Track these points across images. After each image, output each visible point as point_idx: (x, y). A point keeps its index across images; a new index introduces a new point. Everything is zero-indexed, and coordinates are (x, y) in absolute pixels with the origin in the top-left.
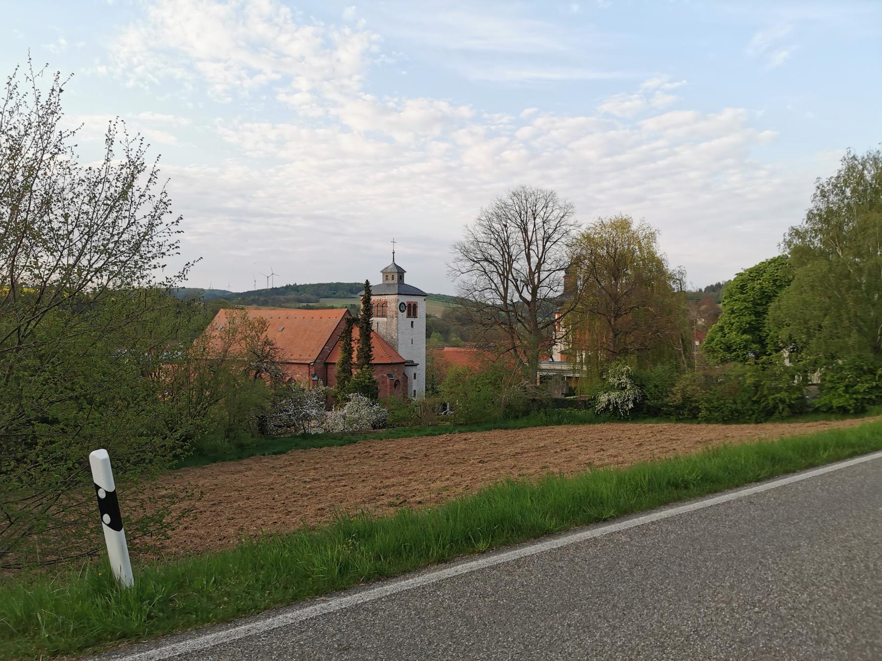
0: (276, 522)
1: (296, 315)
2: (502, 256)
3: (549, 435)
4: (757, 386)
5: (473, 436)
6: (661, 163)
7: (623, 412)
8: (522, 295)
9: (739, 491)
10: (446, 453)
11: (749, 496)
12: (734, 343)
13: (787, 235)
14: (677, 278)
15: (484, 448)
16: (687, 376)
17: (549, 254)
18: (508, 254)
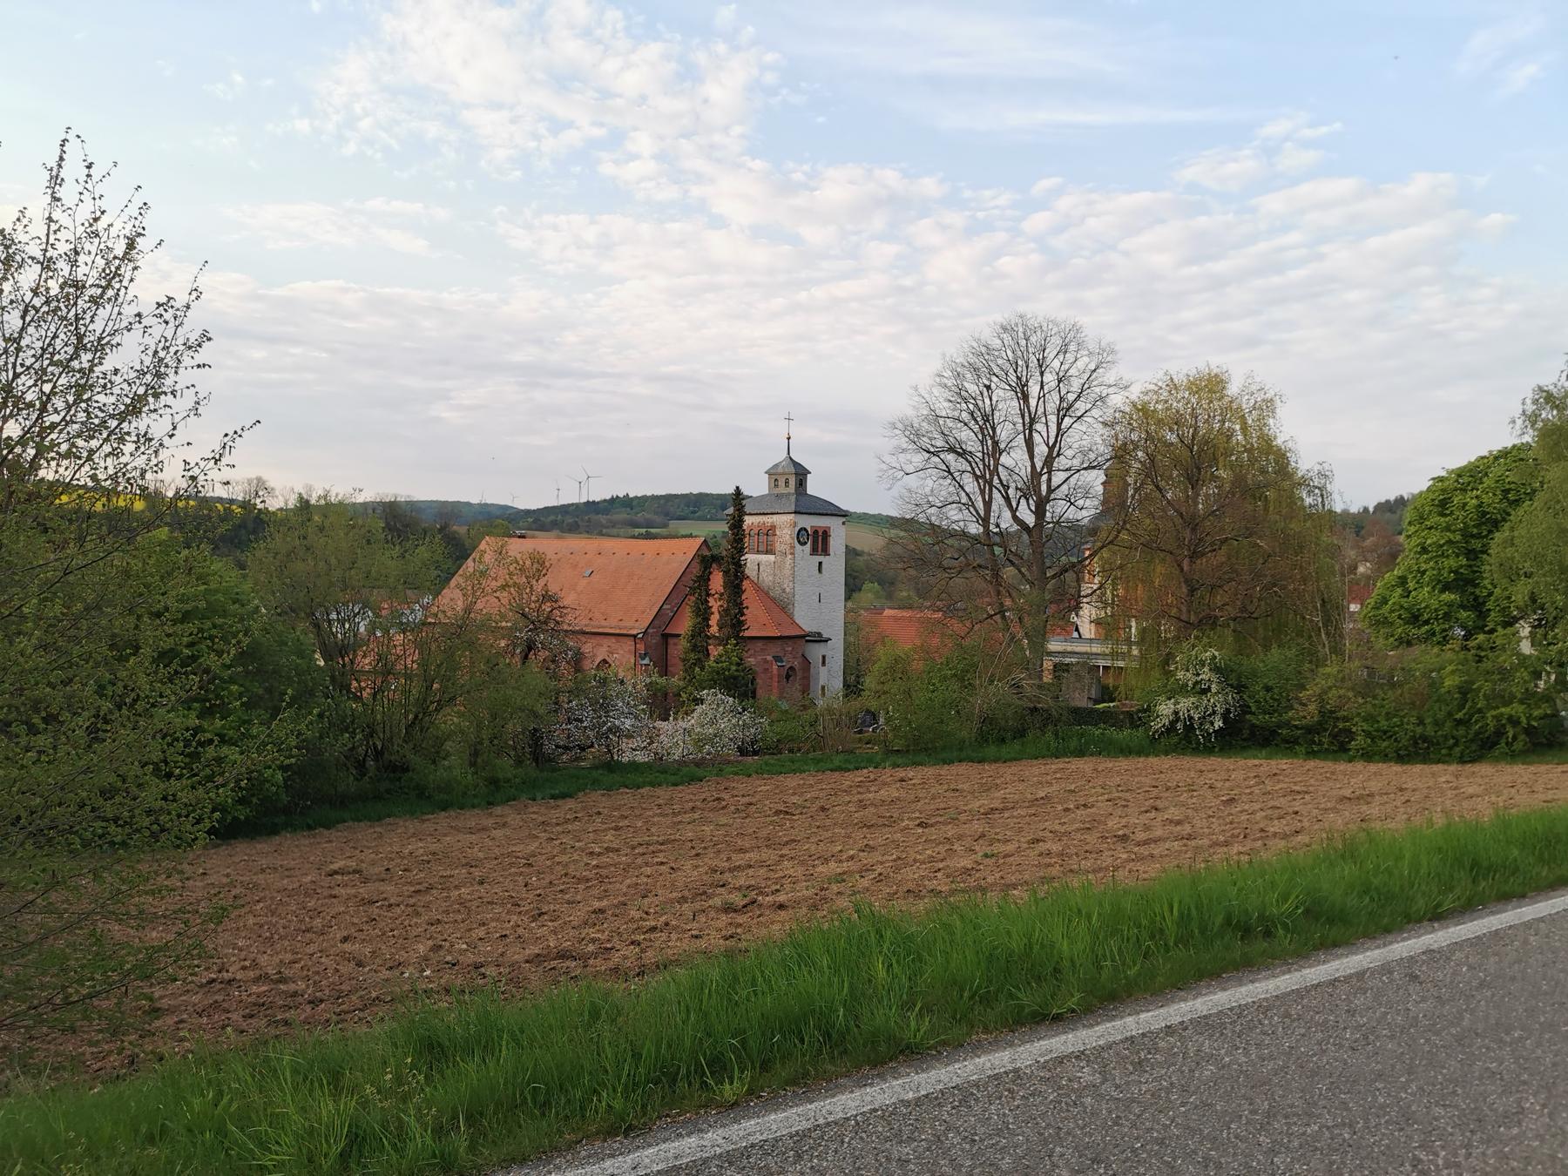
0: (505, 936)
1: (617, 548)
2: (982, 442)
3: (1058, 776)
4: (1465, 691)
5: (913, 773)
6: (1295, 275)
7: (1203, 736)
8: (1017, 514)
9: (1391, 943)
10: (862, 805)
11: (1412, 957)
12: (1425, 608)
13: (1529, 401)
14: (1316, 484)
15: (934, 798)
16: (1328, 670)
17: (1068, 440)
18: (992, 438)
